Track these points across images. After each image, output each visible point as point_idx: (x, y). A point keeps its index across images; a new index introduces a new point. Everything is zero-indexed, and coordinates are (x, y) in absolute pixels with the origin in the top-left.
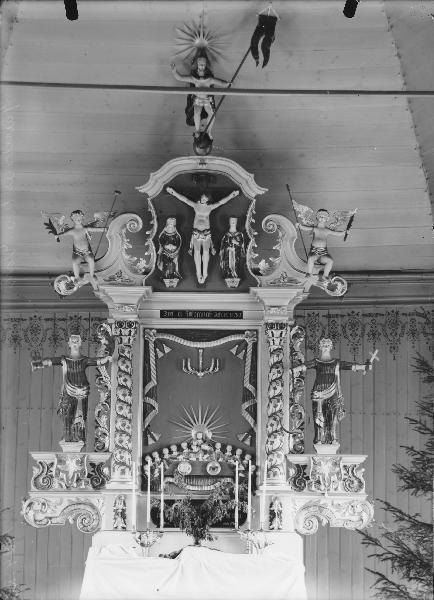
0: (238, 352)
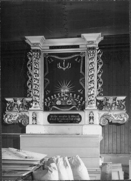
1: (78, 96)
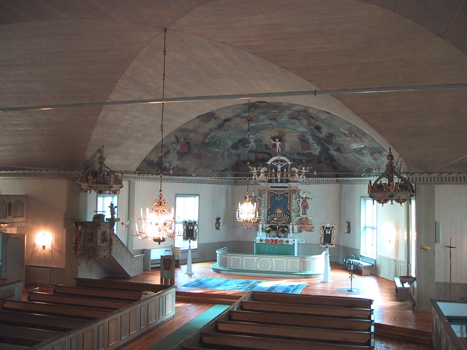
1: (287, 216)
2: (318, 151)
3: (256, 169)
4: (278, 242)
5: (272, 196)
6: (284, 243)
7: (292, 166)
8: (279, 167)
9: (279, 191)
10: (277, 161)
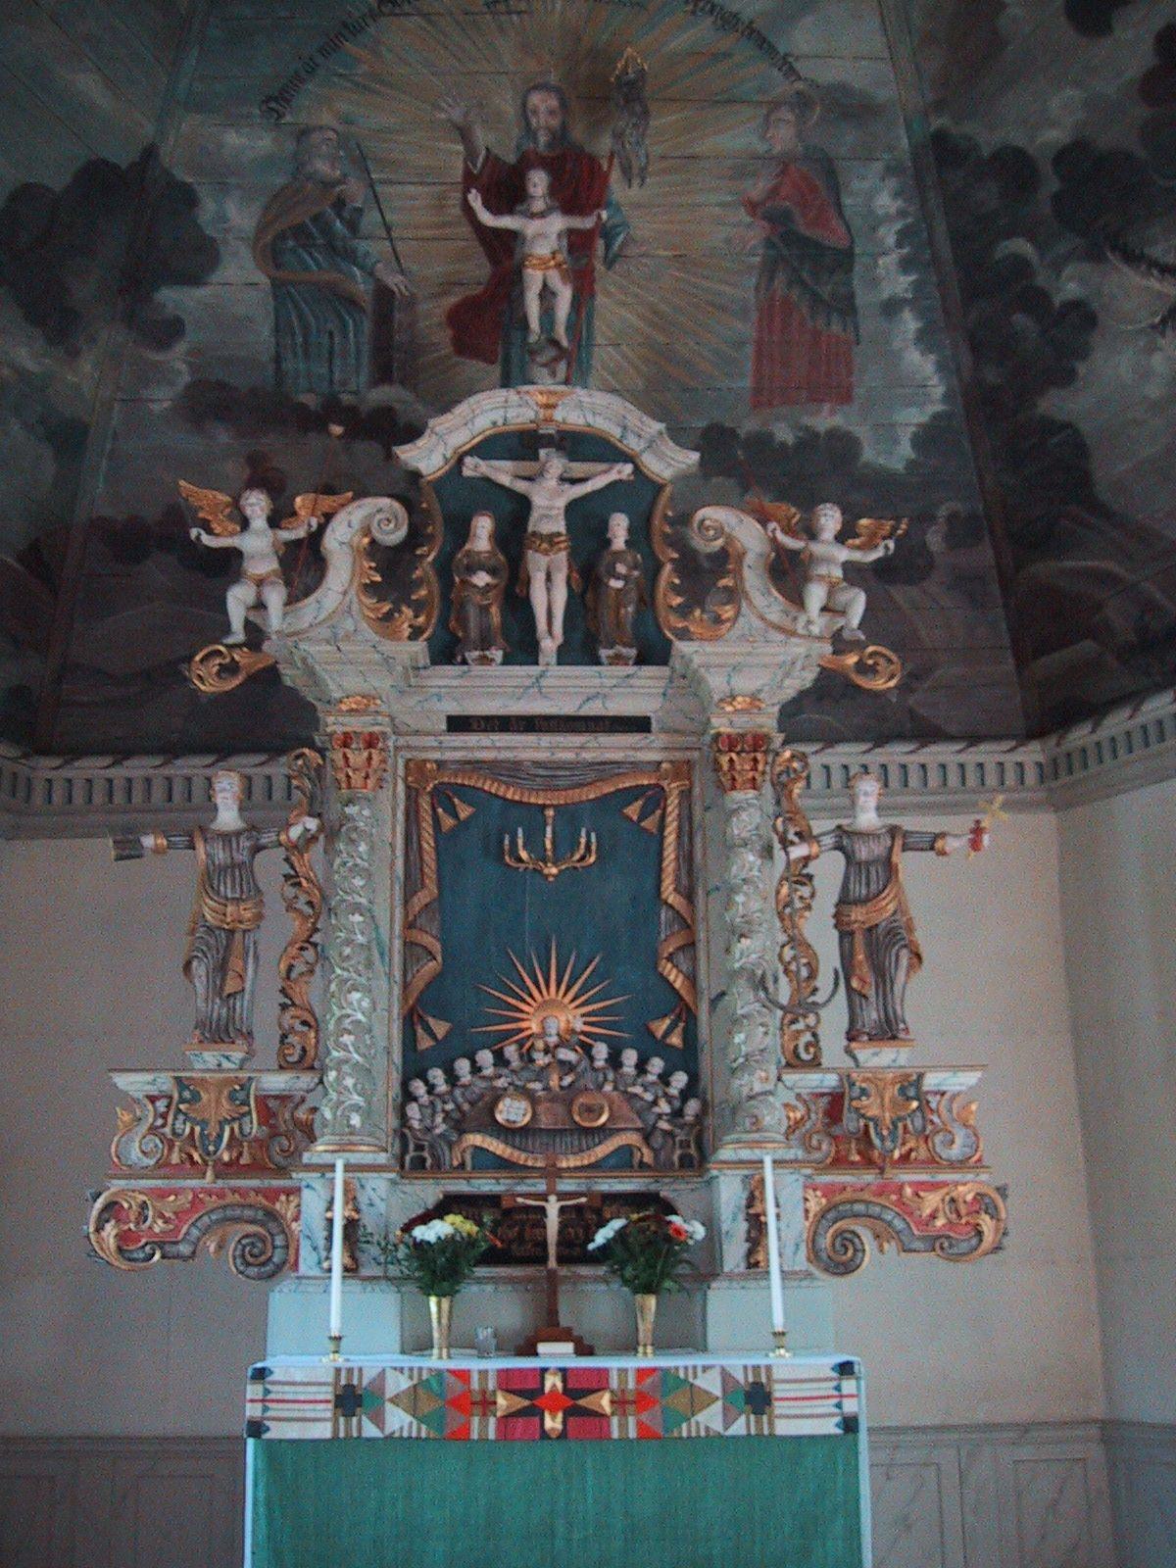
0: (643, 816)
1: (656, 1065)
2: (914, 417)
3: (274, 522)
4: (619, 1403)
5: (463, 825)
6: (710, 1419)
7: (695, 490)
8: (550, 503)
9: (550, 773)
10: (523, 444)
